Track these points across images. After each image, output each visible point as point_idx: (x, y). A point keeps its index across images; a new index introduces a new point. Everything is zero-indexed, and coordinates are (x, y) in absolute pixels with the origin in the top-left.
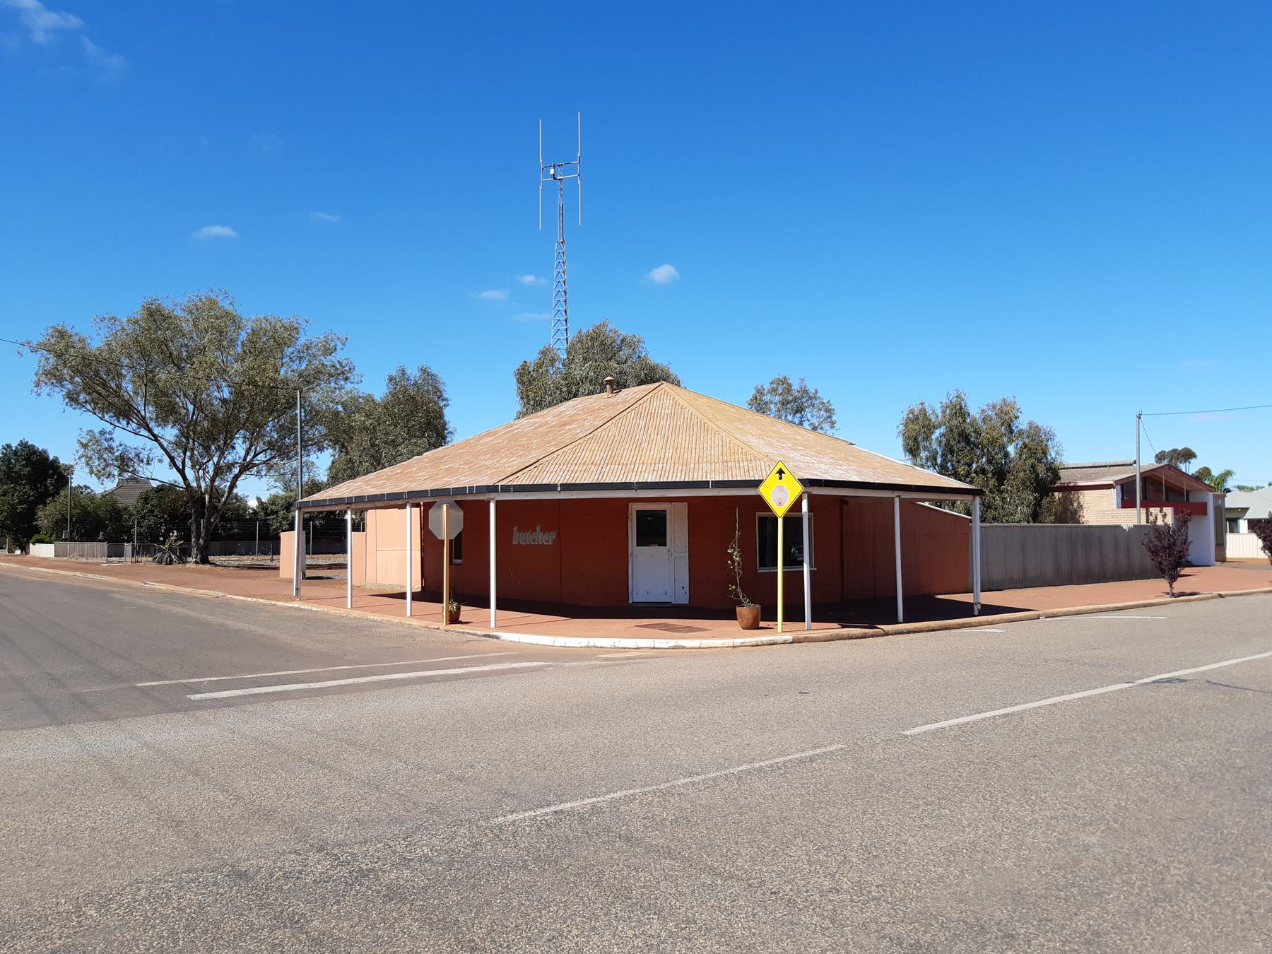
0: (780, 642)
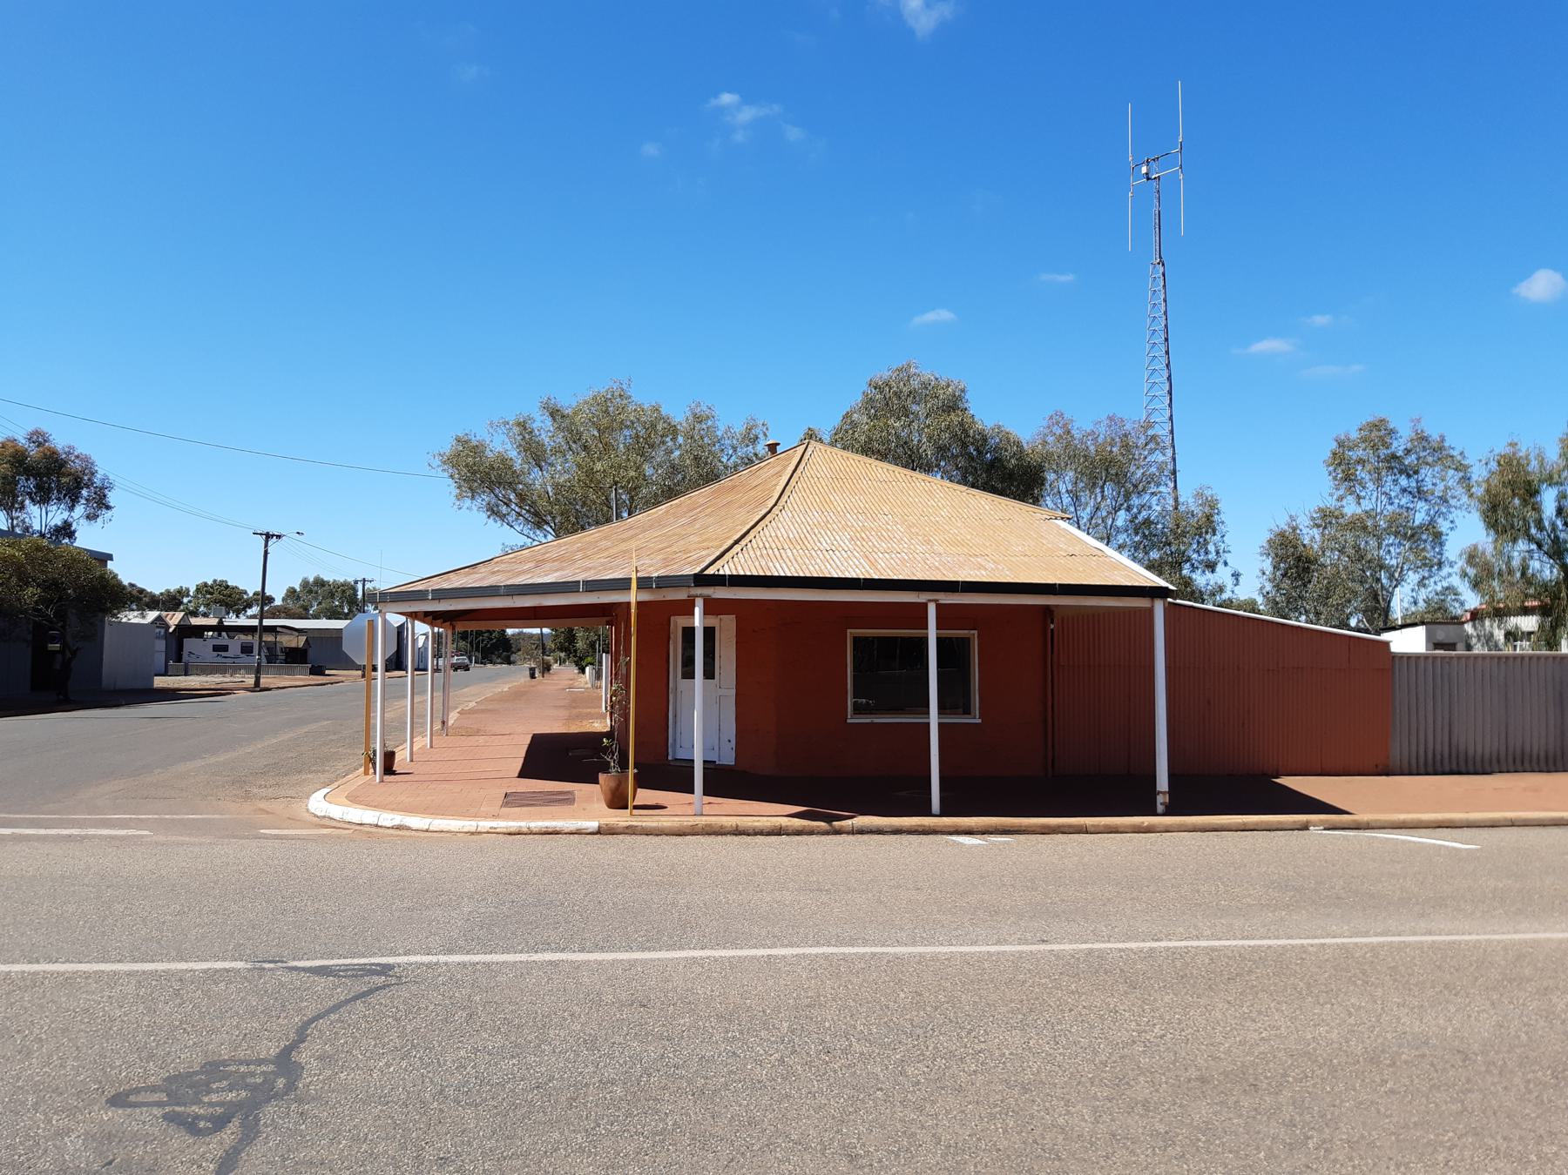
0: (566, 831)
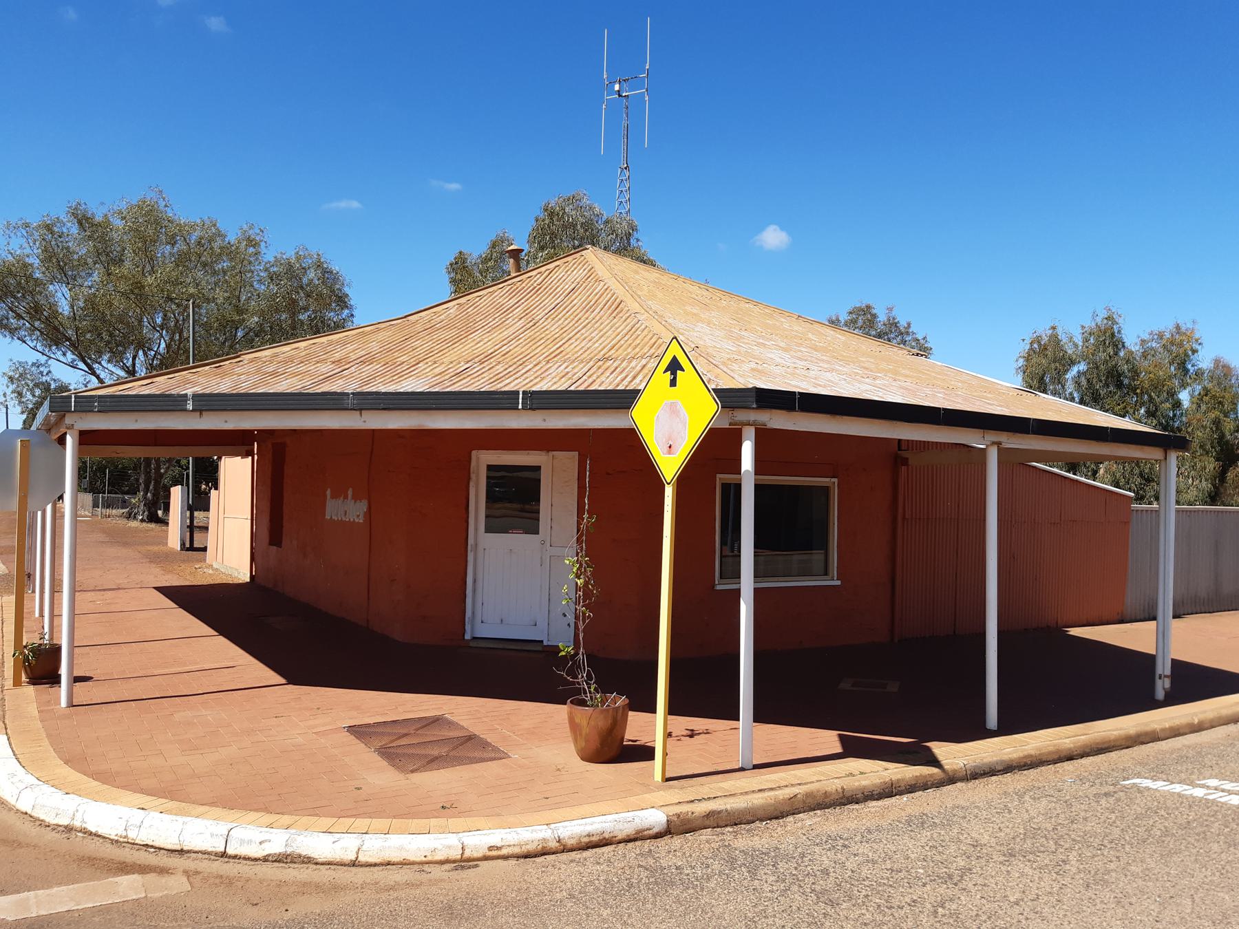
0: (620, 837)
